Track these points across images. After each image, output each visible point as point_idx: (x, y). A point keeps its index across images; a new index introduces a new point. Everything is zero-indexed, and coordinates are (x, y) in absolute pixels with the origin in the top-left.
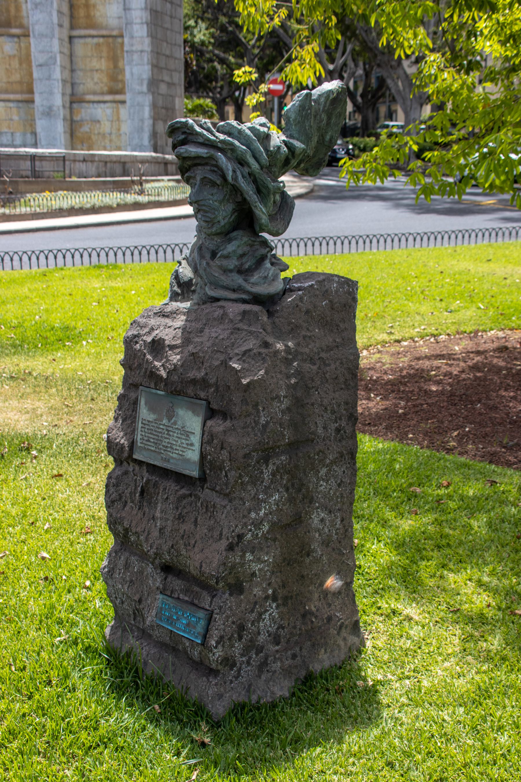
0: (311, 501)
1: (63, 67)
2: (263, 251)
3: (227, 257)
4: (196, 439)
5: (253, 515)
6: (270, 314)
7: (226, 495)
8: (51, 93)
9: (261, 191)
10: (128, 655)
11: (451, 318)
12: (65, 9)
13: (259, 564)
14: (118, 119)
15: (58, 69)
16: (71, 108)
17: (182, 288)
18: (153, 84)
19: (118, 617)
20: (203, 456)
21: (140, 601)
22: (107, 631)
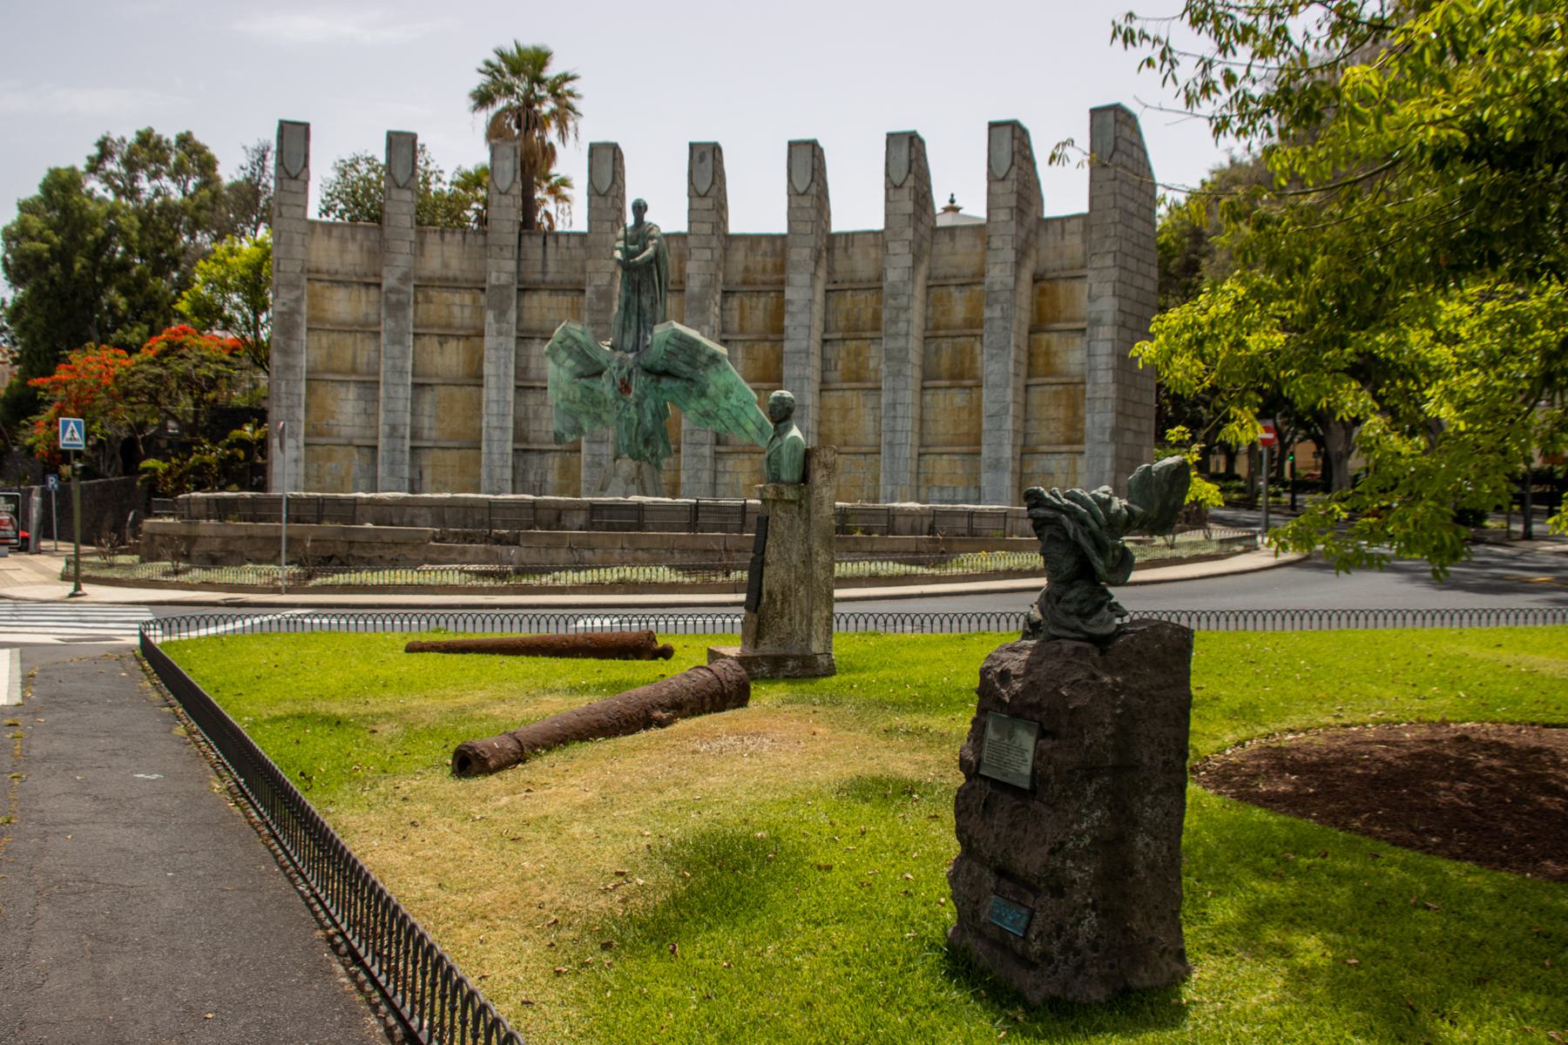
0: (1136, 824)
1: (1016, 417)
2: (1103, 598)
3: (1069, 602)
4: (1029, 756)
5: (1075, 827)
6: (1103, 652)
7: (1052, 806)
8: (1000, 444)
9: (1100, 548)
10: (965, 950)
11: (1418, 705)
12: (1023, 358)
13: (1081, 873)
14: (1075, 472)
15: (1010, 420)
16: (1021, 460)
17: (1033, 628)
18: (1117, 432)
19: (960, 920)
20: (1034, 770)
21: (977, 902)
22: (950, 931)
